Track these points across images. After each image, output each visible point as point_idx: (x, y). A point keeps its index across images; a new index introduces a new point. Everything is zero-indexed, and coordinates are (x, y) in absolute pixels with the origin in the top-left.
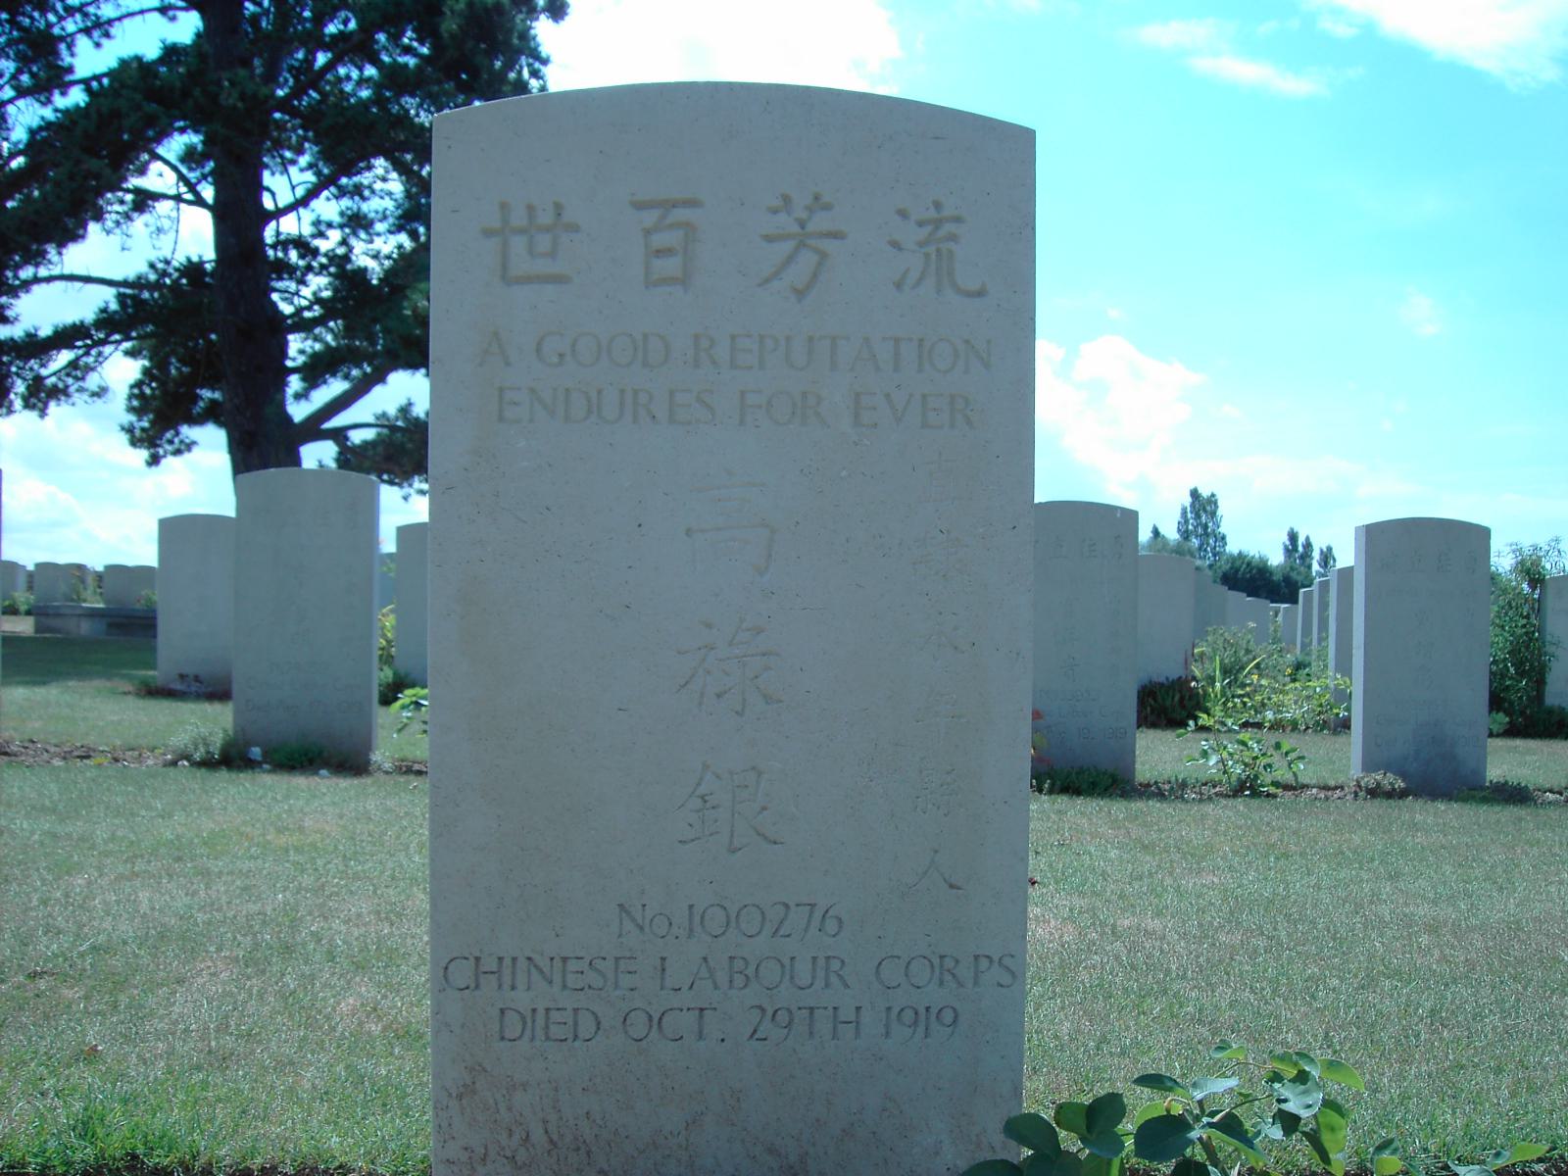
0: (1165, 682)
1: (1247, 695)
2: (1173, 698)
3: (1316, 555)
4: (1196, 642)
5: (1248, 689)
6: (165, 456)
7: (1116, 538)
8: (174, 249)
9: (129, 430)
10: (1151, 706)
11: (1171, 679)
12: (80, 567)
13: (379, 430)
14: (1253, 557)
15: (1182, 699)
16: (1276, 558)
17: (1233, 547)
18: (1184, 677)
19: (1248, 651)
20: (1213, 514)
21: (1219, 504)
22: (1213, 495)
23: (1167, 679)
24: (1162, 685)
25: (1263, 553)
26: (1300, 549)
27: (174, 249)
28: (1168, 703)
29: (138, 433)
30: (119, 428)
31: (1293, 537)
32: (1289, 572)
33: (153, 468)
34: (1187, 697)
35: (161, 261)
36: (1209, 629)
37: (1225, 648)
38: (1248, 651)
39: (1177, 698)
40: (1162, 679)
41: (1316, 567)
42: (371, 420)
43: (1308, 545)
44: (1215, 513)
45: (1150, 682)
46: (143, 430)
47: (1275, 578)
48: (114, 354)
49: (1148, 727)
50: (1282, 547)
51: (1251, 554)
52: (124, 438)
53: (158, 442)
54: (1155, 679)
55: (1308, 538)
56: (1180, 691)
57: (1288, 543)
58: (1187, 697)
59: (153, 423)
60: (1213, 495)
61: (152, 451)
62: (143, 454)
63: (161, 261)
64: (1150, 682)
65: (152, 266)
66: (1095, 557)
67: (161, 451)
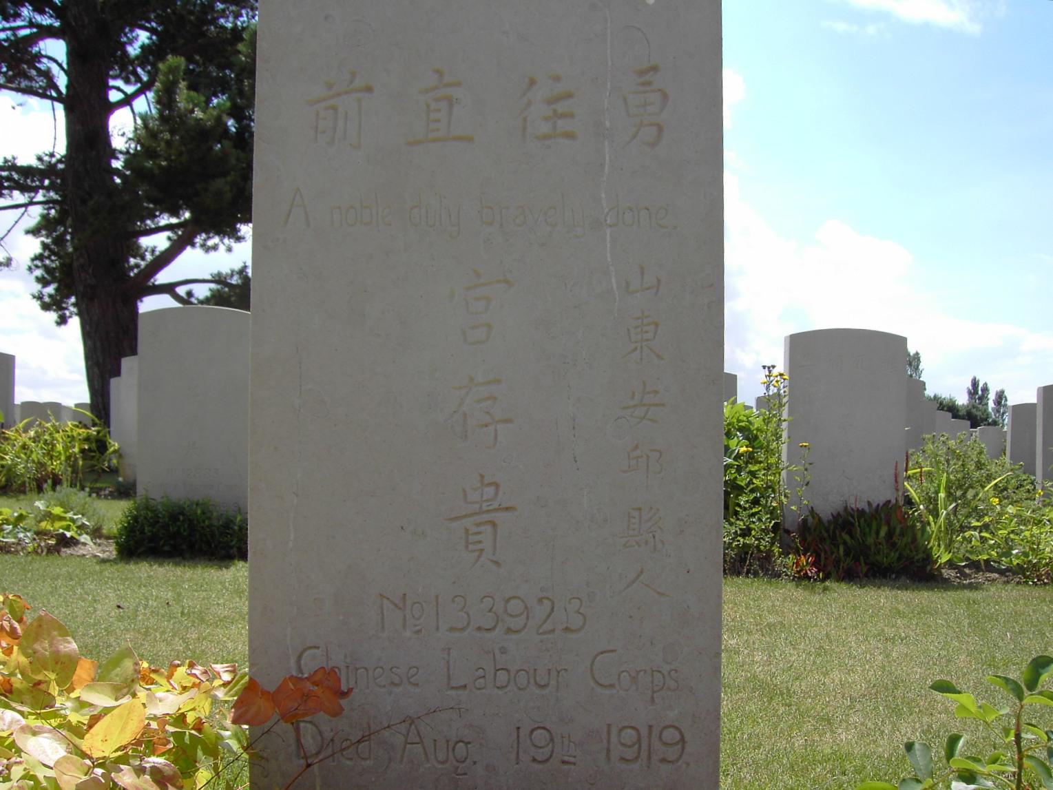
0: (867, 509)
1: (986, 527)
2: (877, 533)
3: (992, 396)
4: (910, 451)
5: (987, 519)
6: (70, 317)
7: (641, 73)
8: (54, 144)
9: (39, 297)
10: (845, 543)
11: (874, 505)
12: (60, 404)
13: (213, 286)
14: (945, 399)
15: (890, 534)
16: (962, 400)
17: (930, 392)
18: (893, 501)
19: (979, 466)
20: (917, 368)
21: (921, 360)
22: (917, 354)
23: (869, 504)
24: (861, 513)
25: (952, 396)
26: (980, 393)
27: (54, 144)
28: (870, 540)
29: (47, 299)
30: (31, 297)
31: (975, 383)
32: (970, 410)
33: (63, 327)
34: (898, 530)
35: (47, 155)
36: (927, 436)
37: (948, 461)
38: (979, 466)
39: (883, 533)
40: (862, 505)
41: (991, 405)
42: (209, 278)
43: (985, 389)
44: (918, 367)
45: (846, 509)
46: (50, 296)
47: (960, 414)
48: (894, 471)
49: (840, 579)
50: (966, 391)
51: (943, 397)
52: (36, 304)
53: (64, 305)
54: (852, 504)
55: (986, 384)
56: (888, 523)
57: (971, 388)
58: (898, 530)
59: (57, 290)
60: (917, 354)
61: (60, 313)
62: (53, 316)
63: (47, 155)
64: (846, 509)
65: (40, 159)
66: (570, 136)
67: (67, 313)
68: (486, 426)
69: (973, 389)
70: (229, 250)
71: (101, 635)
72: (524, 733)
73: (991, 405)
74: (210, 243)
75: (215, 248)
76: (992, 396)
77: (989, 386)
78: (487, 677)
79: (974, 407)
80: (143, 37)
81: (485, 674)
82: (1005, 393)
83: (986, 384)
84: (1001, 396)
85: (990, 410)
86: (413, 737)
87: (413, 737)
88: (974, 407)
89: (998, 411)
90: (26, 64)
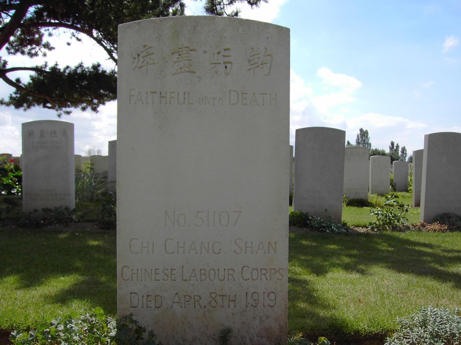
3: (400, 149)
20: (367, 137)
22: (367, 131)
26: (395, 148)
31: (392, 144)
41: (400, 153)
43: (398, 146)
51: (379, 150)
55: (398, 144)
57: (391, 146)
60: (367, 131)
68: (185, 99)
69: (392, 146)
70: (45, 55)
71: (324, 230)
72: (249, 295)
73: (400, 153)
74: (33, 52)
75: (36, 54)
76: (400, 149)
77: (399, 145)
78: (236, 301)
79: (393, 154)
80: (86, 83)
81: (235, 299)
82: (406, 148)
83: (398, 144)
84: (404, 150)
85: (399, 155)
86: (193, 275)
87: (193, 275)
88: (393, 154)
89: (403, 156)
90: (69, 102)
